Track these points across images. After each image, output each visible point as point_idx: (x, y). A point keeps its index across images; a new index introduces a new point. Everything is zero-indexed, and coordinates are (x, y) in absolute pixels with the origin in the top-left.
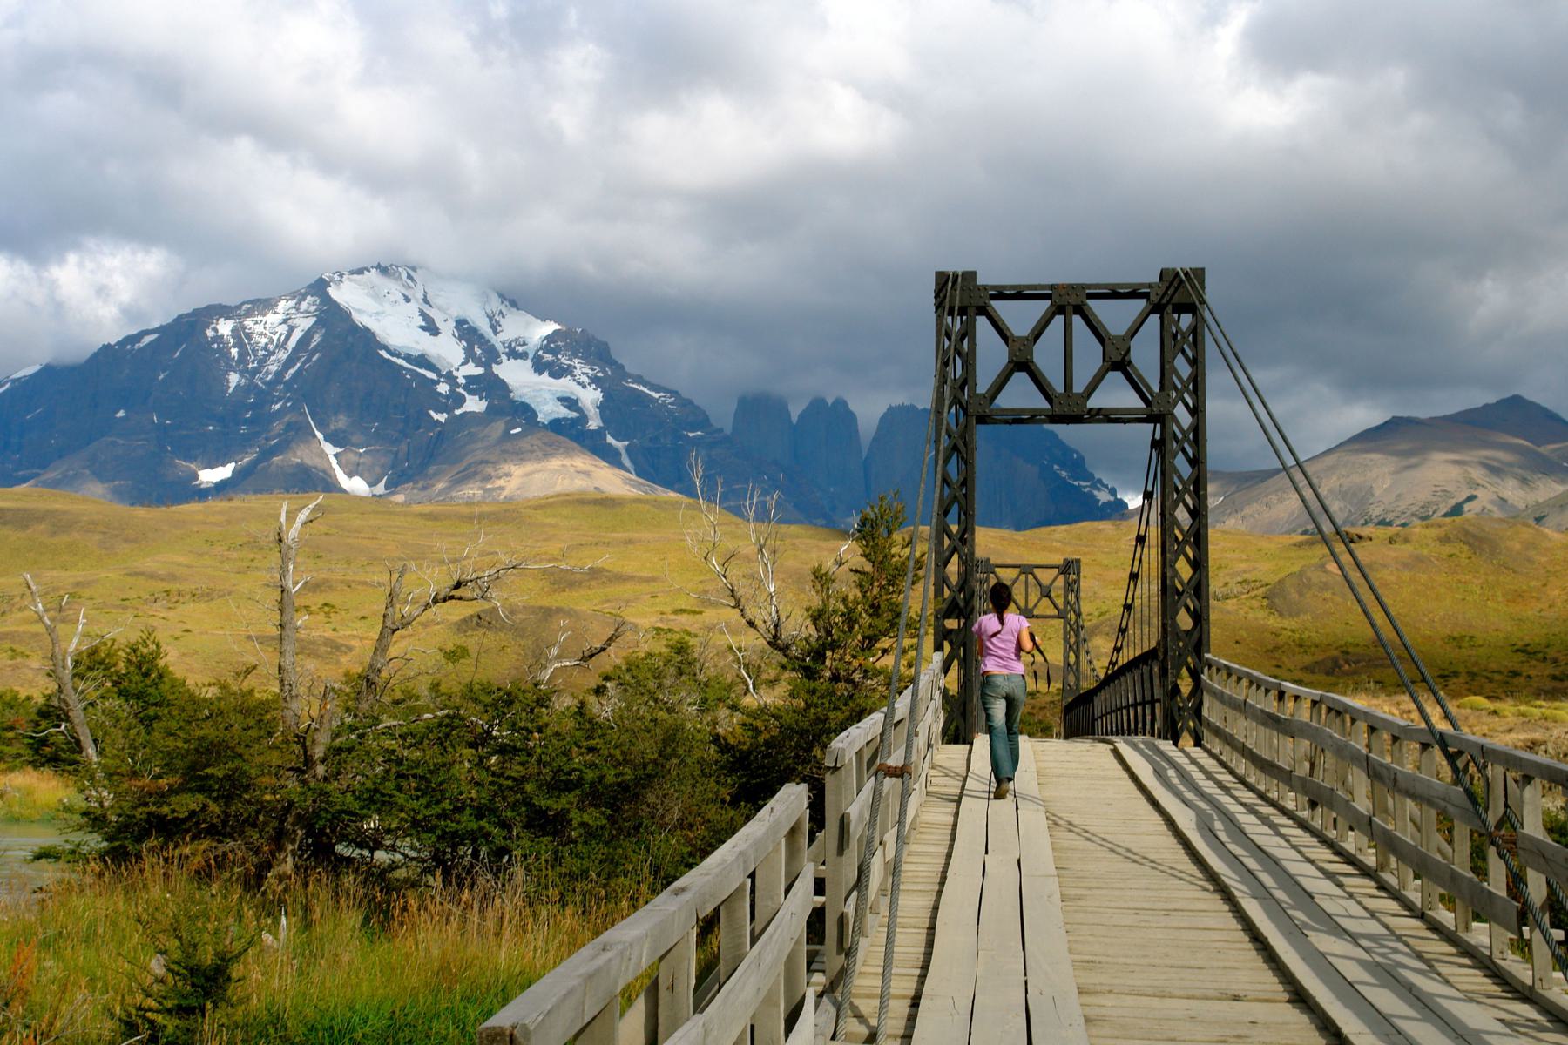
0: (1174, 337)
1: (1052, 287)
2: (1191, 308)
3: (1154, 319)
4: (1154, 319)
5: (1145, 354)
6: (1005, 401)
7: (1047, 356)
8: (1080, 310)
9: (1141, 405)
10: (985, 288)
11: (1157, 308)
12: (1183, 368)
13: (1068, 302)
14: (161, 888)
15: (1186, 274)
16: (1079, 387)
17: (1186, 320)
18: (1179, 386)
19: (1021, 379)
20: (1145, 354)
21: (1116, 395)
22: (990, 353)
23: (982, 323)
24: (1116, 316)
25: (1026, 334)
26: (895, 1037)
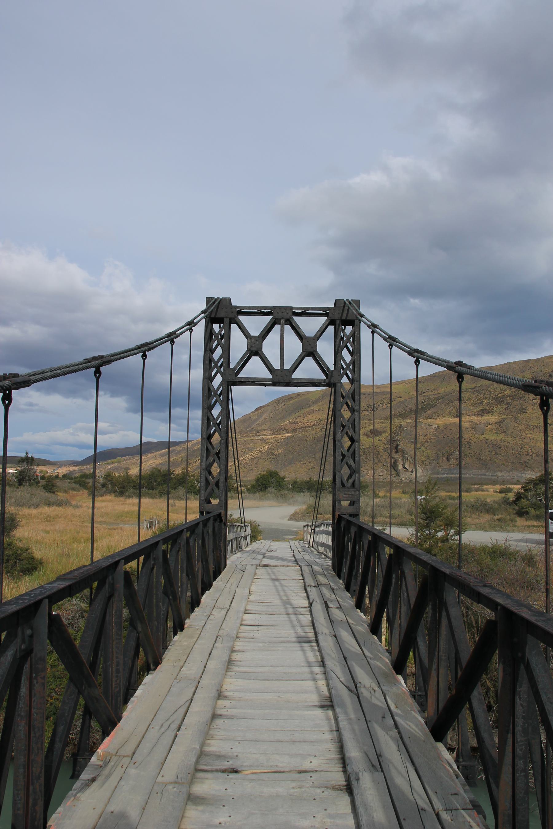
0: (342, 338)
1: (274, 308)
2: (351, 323)
3: (331, 328)
4: (331, 328)
5: (326, 349)
6: (297, 375)
7: (294, 346)
8: (290, 322)
9: (324, 377)
10: (236, 307)
11: (332, 322)
12: (347, 356)
13: (282, 317)
14: (507, 497)
15: (350, 303)
16: (287, 367)
17: (349, 329)
18: (345, 367)
19: (309, 362)
20: (326, 349)
21: (309, 369)
22: (239, 344)
23: (234, 326)
24: (310, 325)
25: (257, 334)
26: (188, 817)
